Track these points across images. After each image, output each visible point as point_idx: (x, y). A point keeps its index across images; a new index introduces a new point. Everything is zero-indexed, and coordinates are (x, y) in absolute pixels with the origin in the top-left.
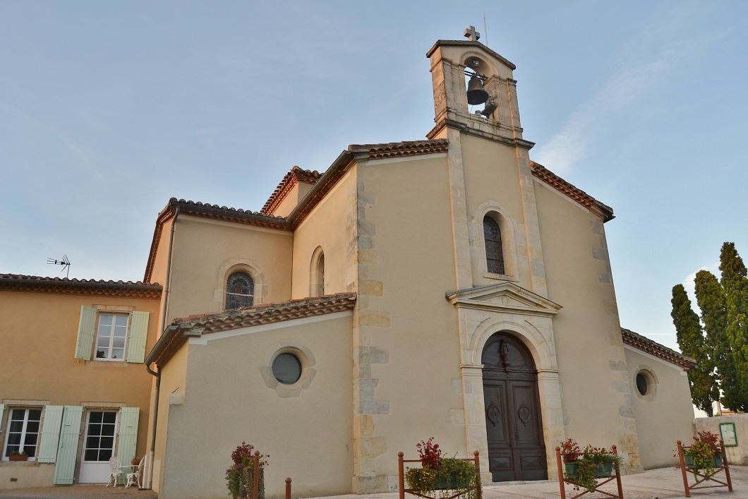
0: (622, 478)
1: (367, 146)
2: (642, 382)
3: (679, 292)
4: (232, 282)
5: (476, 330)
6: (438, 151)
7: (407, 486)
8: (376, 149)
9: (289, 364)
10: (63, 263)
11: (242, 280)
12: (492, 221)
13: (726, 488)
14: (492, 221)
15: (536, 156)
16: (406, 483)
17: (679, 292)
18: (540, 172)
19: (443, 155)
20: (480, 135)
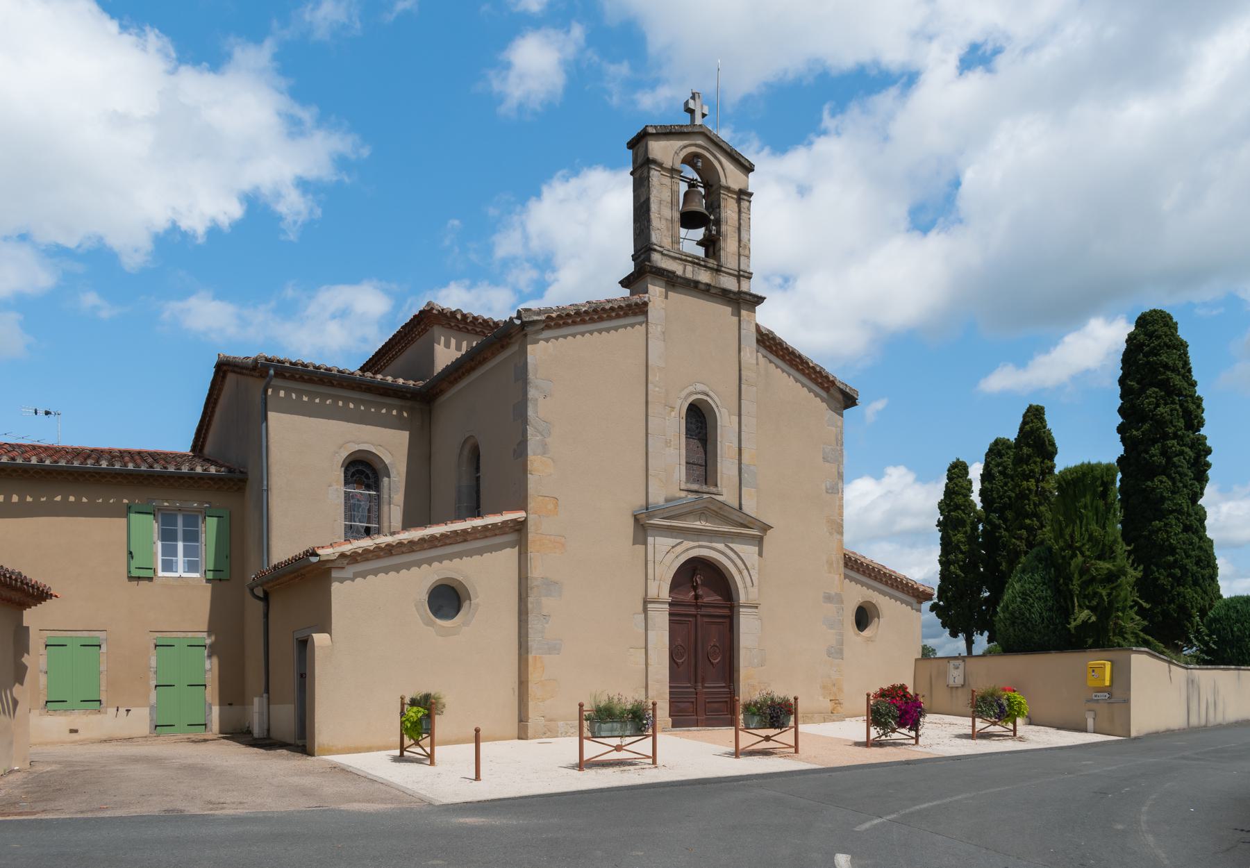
0: (482, 745)
1: (539, 312)
2: (864, 617)
3: (958, 471)
4: (350, 474)
5: (668, 554)
6: (635, 314)
7: (587, 733)
8: (554, 315)
9: (864, 617)
10: (47, 413)
11: (362, 472)
12: (699, 420)
13: (913, 741)
14: (699, 420)
15: (768, 317)
16: (585, 730)
17: (958, 471)
18: (769, 343)
19: (641, 318)
20: (692, 287)
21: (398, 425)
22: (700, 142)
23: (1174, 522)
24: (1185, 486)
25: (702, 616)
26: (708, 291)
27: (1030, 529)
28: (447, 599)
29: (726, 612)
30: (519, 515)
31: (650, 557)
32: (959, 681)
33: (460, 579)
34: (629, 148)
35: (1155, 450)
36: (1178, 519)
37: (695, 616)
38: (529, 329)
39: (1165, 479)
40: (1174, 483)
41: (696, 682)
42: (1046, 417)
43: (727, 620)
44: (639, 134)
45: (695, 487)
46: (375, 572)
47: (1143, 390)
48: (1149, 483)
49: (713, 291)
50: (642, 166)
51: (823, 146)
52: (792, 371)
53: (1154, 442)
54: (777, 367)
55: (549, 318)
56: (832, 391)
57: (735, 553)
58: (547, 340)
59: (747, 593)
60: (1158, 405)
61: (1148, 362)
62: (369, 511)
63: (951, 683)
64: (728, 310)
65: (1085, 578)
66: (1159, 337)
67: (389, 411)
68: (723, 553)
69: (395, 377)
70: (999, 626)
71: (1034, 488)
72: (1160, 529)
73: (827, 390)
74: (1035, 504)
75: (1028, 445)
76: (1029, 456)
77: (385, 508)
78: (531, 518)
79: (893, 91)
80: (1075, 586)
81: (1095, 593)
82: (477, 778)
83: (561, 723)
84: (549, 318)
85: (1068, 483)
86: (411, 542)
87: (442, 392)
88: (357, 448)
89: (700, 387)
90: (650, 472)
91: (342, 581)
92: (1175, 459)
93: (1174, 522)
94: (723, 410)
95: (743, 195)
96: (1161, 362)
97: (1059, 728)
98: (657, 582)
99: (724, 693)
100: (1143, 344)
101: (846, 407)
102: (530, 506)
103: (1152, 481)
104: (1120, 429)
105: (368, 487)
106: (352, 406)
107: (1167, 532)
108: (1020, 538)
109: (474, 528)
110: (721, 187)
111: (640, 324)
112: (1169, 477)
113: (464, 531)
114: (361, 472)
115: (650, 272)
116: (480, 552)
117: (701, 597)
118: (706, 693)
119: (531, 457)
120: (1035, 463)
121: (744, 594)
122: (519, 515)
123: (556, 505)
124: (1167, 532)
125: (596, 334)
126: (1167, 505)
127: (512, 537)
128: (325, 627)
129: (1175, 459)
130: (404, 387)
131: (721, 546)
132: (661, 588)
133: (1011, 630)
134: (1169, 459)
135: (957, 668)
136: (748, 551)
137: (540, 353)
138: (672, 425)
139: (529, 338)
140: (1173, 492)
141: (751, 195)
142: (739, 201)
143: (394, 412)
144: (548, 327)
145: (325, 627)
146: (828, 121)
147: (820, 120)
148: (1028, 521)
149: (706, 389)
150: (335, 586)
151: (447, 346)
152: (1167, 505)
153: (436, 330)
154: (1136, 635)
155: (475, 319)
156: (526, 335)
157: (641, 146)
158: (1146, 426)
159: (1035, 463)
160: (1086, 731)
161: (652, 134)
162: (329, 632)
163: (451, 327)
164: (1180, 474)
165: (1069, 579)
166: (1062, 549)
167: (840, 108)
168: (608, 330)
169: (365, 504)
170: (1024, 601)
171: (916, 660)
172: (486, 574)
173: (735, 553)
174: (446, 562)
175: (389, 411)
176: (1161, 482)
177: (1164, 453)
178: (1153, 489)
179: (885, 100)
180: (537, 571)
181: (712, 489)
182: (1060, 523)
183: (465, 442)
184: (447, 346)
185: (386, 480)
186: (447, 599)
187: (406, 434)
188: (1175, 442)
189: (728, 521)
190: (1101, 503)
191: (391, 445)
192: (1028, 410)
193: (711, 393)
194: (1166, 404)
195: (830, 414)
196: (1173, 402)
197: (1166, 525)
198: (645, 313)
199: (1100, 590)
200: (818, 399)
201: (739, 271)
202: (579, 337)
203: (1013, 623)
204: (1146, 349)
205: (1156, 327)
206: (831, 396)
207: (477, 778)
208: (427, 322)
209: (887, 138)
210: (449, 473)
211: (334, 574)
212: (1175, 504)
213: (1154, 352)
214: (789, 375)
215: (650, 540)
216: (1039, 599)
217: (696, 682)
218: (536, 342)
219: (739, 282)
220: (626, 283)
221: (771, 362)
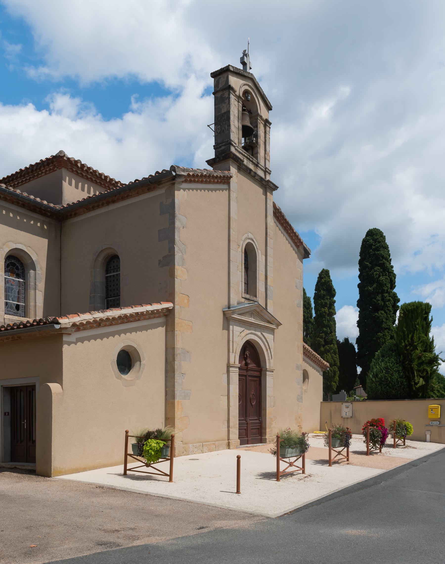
5: (240, 336)
8: (191, 174)
12: (249, 254)
14: (249, 254)
18: (279, 215)
19: (226, 186)
21: (41, 234)
22: (250, 84)
23: (387, 334)
24: (391, 317)
25: (249, 376)
26: (254, 177)
27: (326, 333)
28: (126, 361)
29: (256, 374)
30: (169, 305)
31: (231, 339)
32: (349, 414)
33: (135, 346)
34: (212, 77)
35: (379, 297)
36: (388, 332)
37: (246, 376)
38: (178, 180)
39: (383, 312)
40: (387, 315)
41: (246, 417)
42: (330, 274)
43: (258, 379)
44: (222, 69)
45: (248, 296)
46: (89, 339)
47: (372, 268)
48: (376, 314)
49: (257, 177)
50: (223, 90)
51: (129, 117)
52: (285, 234)
53: (378, 293)
54: (280, 230)
55: (189, 175)
56: (301, 248)
57: (265, 338)
58: (184, 190)
59: (270, 363)
60: (380, 276)
61: (375, 254)
62: (18, 292)
63: (344, 415)
64: (260, 191)
65: (420, 361)
66: (379, 242)
67: (35, 223)
68: (260, 338)
69: (42, 199)
70: (368, 385)
71: (328, 312)
72: (381, 337)
73: (298, 247)
74: (328, 320)
75: (324, 290)
76: (324, 295)
77: (32, 292)
78: (177, 307)
79: (170, 98)
80: (415, 365)
81: (424, 370)
82: (238, 492)
83: (191, 445)
84: (189, 175)
85: (408, 311)
86: (114, 319)
87: (76, 215)
88: (14, 246)
89: (250, 236)
90: (231, 285)
91: (69, 344)
92: (387, 303)
93: (387, 334)
94: (259, 251)
95: (267, 123)
96: (381, 254)
97: (411, 440)
98: (234, 354)
99: (256, 423)
100: (372, 245)
101: (305, 258)
102: (176, 299)
103: (378, 313)
104: (359, 286)
105: (18, 276)
106: (11, 215)
107: (384, 338)
108: (321, 338)
109: (147, 311)
110: (258, 115)
111: (226, 190)
112: (385, 312)
113: (142, 313)
114: (13, 264)
115: (233, 158)
116: (146, 328)
117: (249, 364)
118: (252, 423)
119: (177, 267)
120: (327, 299)
121: (270, 363)
122: (169, 305)
123: (188, 300)
124: (384, 338)
125: (191, 190)
126: (384, 325)
127: (161, 320)
128: (59, 379)
129: (387, 303)
130: (47, 207)
131: (259, 334)
132: (235, 358)
133: (380, 387)
134: (385, 302)
135: (348, 407)
136: (269, 336)
137: (182, 196)
138: (238, 257)
139: (176, 186)
140: (387, 319)
141: (270, 124)
142: (265, 126)
143: (39, 224)
144: (186, 181)
145: (59, 379)
146: (135, 106)
147: (130, 103)
148: (325, 329)
149: (252, 237)
150: (65, 348)
151: (70, 184)
152: (384, 325)
153: (64, 171)
154: (438, 391)
155: (89, 168)
156: (174, 184)
157: (222, 79)
158: (375, 285)
159: (327, 299)
160: (425, 441)
161: (231, 71)
162: (61, 384)
163: (73, 171)
164: (388, 310)
165: (411, 361)
166: (406, 346)
167: (140, 99)
168: (212, 190)
169: (16, 288)
170: (387, 372)
171: (321, 402)
172: (149, 342)
173: (265, 338)
174: (128, 334)
175: (35, 223)
176: (382, 314)
177: (383, 299)
178: (378, 317)
179: (165, 102)
180: (180, 343)
181: (254, 299)
182: (404, 332)
183: (102, 251)
184: (70, 184)
185: (32, 272)
186: (126, 361)
187: (46, 241)
188: (387, 294)
189: (263, 319)
190: (425, 323)
191: (36, 247)
192: (322, 272)
193: (254, 240)
194: (383, 276)
195: (298, 261)
196: (386, 275)
197: (384, 335)
198: (229, 184)
199: (426, 368)
200: (294, 252)
201: (266, 168)
202: (191, 190)
203: (380, 384)
204: (373, 247)
205: (378, 237)
206: (299, 251)
207: (238, 492)
208: (59, 163)
209: (164, 120)
210: (85, 272)
211: (65, 338)
212: (388, 325)
213: (377, 249)
214: (284, 235)
215: (231, 327)
216: (396, 371)
217: (246, 417)
218: (179, 190)
219: (265, 175)
220: (209, 162)
221: (277, 226)
